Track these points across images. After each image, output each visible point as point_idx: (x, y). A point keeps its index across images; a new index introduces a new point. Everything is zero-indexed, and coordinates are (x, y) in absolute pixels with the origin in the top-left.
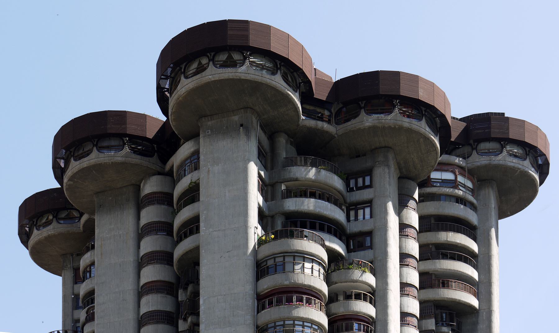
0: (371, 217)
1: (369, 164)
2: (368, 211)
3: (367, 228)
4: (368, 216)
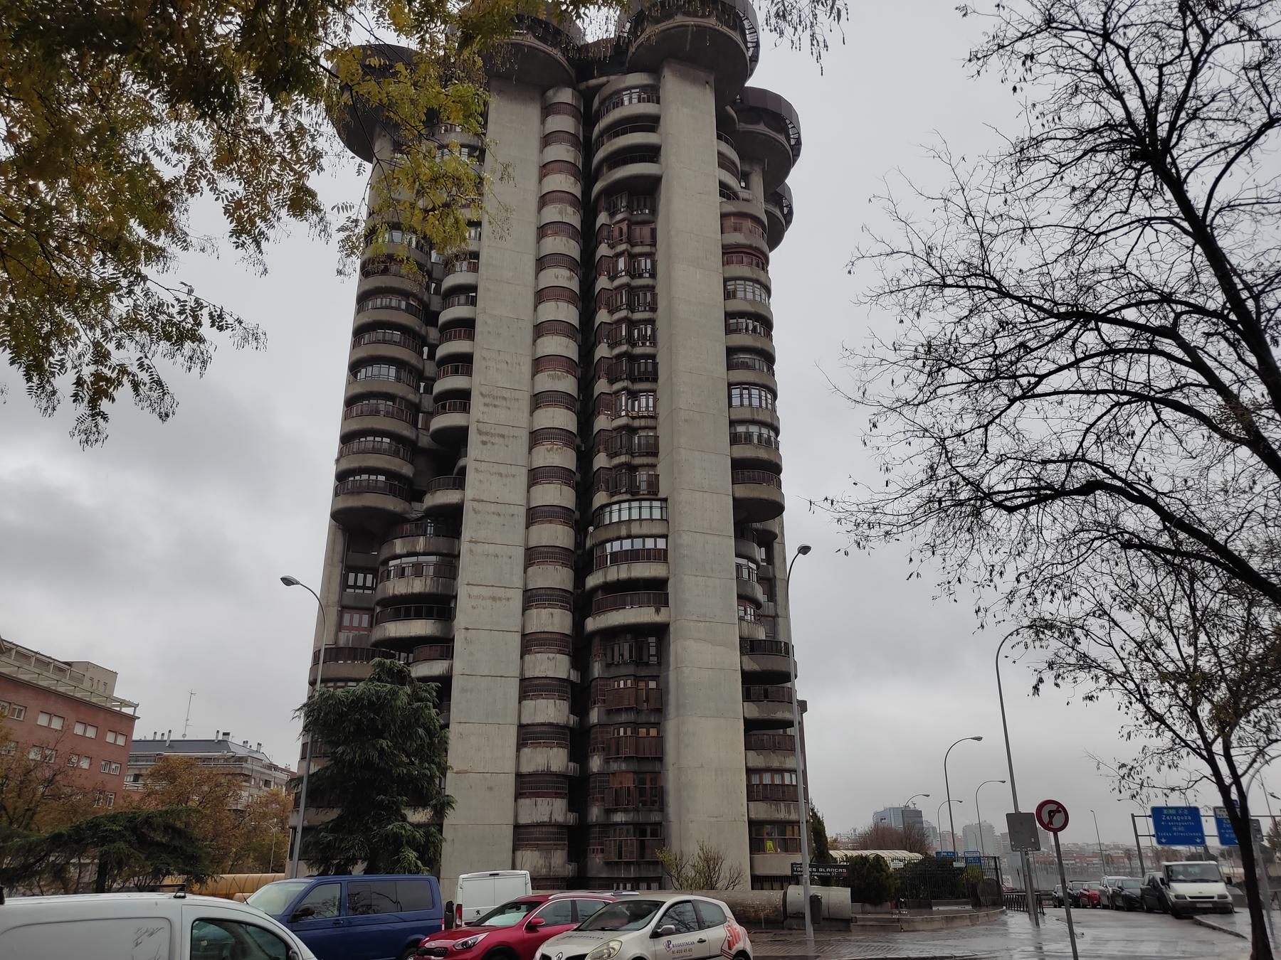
2: (649, 261)
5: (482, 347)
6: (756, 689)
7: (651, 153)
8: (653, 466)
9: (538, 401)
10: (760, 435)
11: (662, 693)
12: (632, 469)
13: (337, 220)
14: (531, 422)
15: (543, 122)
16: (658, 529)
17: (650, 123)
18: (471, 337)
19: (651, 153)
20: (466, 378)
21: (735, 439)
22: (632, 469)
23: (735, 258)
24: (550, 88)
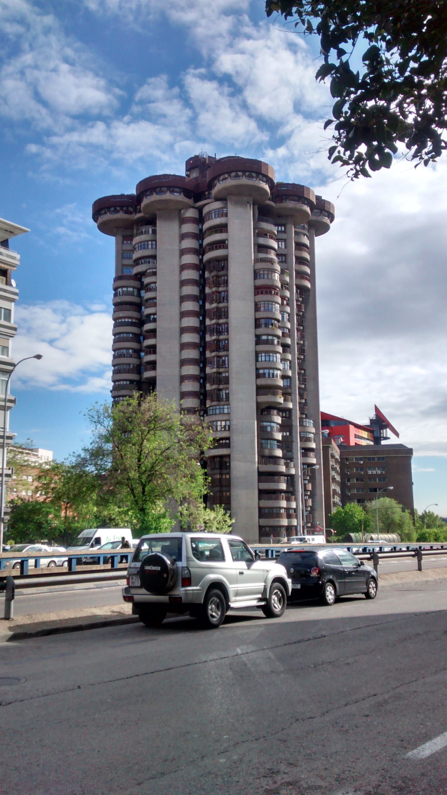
0: (285, 247)
1: (284, 222)
2: (283, 243)
3: (284, 253)
4: (283, 247)
5: (160, 342)
6: (263, 478)
7: (222, 244)
8: (227, 389)
9: (183, 363)
10: (269, 374)
11: (229, 480)
12: (220, 390)
13: (240, 97)
14: (180, 372)
15: (180, 227)
16: (226, 417)
17: (223, 228)
18: (155, 337)
19: (222, 244)
20: (154, 355)
21: (258, 376)
22: (220, 390)
23: (260, 291)
24: (183, 209)
